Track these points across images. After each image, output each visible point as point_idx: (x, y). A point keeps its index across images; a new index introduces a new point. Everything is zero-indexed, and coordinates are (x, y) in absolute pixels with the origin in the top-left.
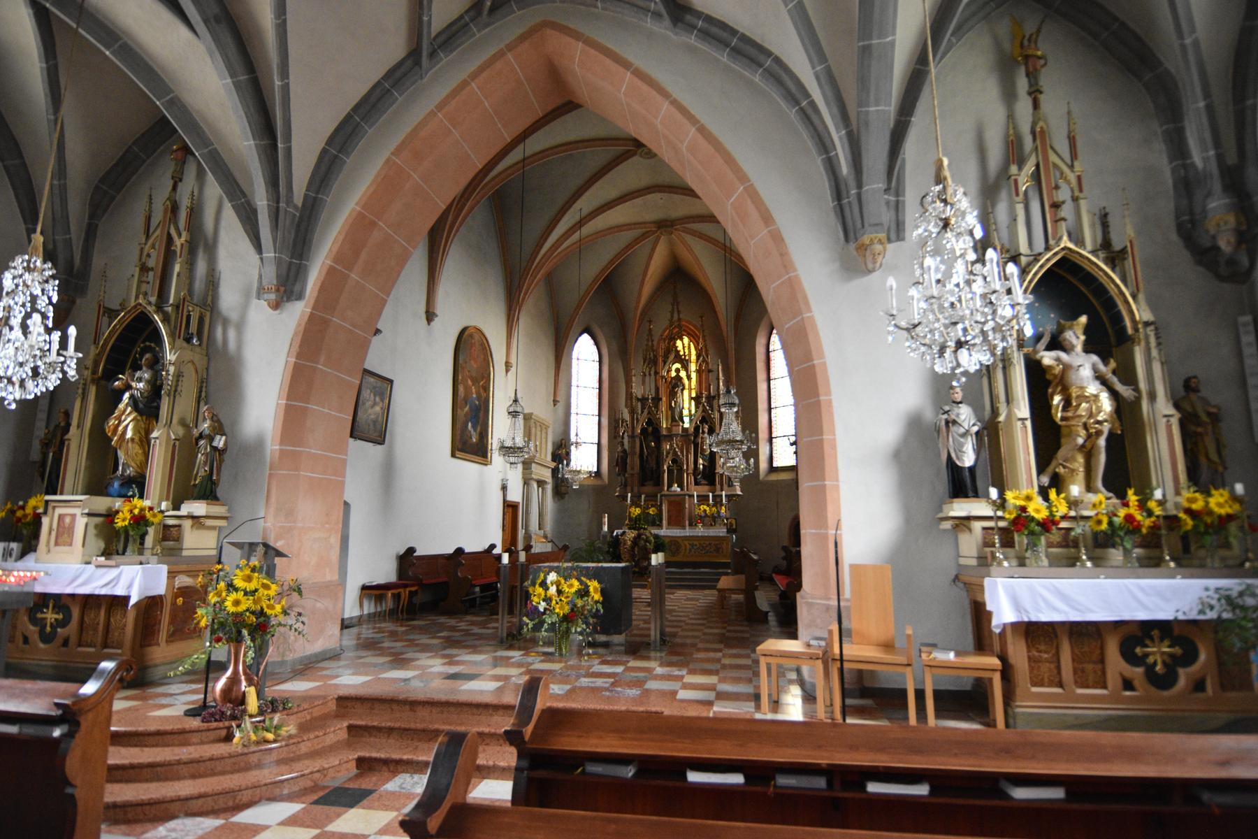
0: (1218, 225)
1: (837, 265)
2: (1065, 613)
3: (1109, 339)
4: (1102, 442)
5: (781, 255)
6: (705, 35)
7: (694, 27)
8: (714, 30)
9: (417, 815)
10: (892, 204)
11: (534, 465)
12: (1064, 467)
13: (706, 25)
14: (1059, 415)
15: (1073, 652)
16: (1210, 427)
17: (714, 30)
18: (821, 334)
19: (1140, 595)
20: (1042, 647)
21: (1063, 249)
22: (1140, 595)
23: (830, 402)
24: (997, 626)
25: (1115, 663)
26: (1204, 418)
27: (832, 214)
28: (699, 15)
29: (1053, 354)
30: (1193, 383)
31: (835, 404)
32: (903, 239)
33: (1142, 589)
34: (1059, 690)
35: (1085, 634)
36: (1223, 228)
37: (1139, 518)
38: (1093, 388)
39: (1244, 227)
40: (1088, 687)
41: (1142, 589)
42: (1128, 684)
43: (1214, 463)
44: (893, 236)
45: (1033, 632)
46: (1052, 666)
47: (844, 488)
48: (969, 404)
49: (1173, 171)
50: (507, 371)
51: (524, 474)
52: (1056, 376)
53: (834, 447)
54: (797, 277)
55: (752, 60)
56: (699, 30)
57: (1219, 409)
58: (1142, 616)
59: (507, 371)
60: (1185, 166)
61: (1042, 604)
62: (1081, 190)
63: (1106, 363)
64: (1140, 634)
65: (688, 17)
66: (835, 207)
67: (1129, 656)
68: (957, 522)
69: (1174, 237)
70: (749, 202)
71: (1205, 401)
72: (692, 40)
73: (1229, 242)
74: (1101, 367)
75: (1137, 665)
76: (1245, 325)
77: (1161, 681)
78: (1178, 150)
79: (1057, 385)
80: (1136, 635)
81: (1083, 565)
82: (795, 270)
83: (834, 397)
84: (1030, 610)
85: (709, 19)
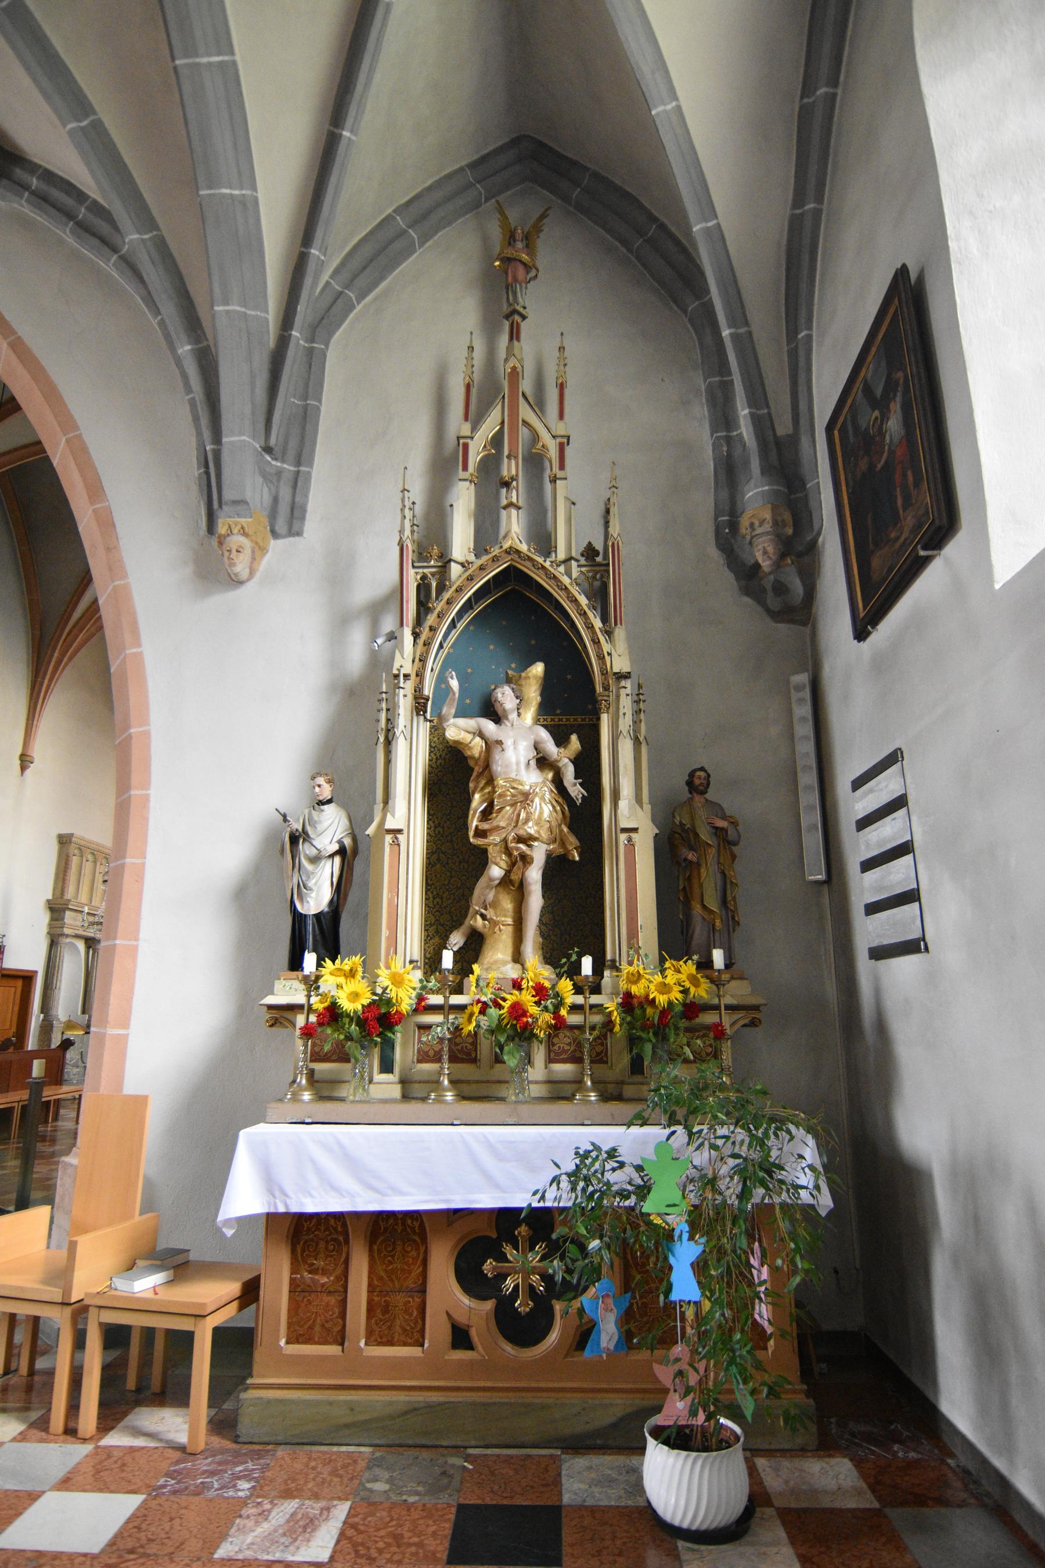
0: (752, 525)
1: (188, 570)
2: (352, 1196)
3: (573, 705)
4: (534, 875)
5: (108, 549)
6: (42, 199)
7: (25, 187)
8: (56, 194)
9: (213, 1412)
10: (287, 477)
11: (68, 913)
12: (484, 917)
13: (44, 187)
14: (475, 823)
15: (371, 1272)
16: (712, 852)
17: (56, 194)
18: (150, 684)
19: (489, 1162)
20: (320, 1263)
21: (508, 552)
22: (489, 1162)
23: (146, 798)
24: (228, 1222)
25: (446, 1294)
26: (705, 835)
27: (195, 488)
28: (32, 168)
29: (471, 723)
30: (700, 778)
31: (153, 803)
32: (299, 534)
33: (490, 1146)
34: (333, 1350)
35: (396, 1235)
36: (759, 531)
37: (534, 1010)
38: (533, 779)
39: (790, 531)
40: (390, 1343)
41: (490, 1146)
42: (461, 1338)
43: (711, 912)
44: (281, 526)
45: (309, 1236)
46: (333, 1300)
47: (145, 949)
48: (343, 806)
49: (715, 447)
50: (23, 768)
51: (51, 926)
52: (477, 760)
53: (140, 878)
54: (126, 588)
55: (104, 241)
56: (33, 193)
57: (735, 824)
58: (487, 1200)
59: (23, 768)
60: (728, 440)
61: (313, 1179)
62: (562, 467)
63: (561, 741)
64: (494, 1235)
65: (19, 173)
66: (200, 477)
67: (470, 1278)
68: (275, 1014)
69: (714, 552)
70: (73, 462)
71: (717, 809)
72: (23, 207)
73: (765, 552)
74: (550, 747)
75: (483, 1298)
76: (799, 688)
77: (522, 1327)
78: (723, 419)
79: (480, 775)
80: (485, 1237)
81: (440, 1100)
82: (125, 576)
83: (152, 792)
84: (289, 1189)
85: (49, 176)
